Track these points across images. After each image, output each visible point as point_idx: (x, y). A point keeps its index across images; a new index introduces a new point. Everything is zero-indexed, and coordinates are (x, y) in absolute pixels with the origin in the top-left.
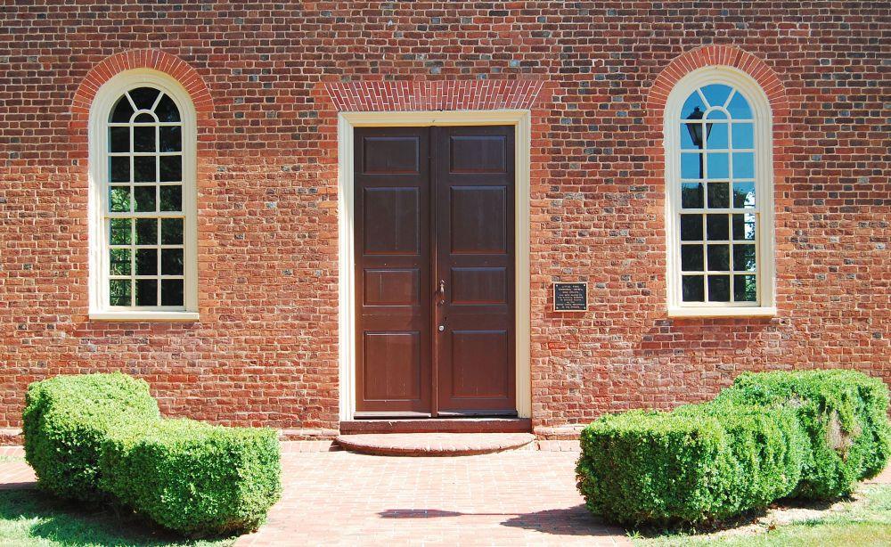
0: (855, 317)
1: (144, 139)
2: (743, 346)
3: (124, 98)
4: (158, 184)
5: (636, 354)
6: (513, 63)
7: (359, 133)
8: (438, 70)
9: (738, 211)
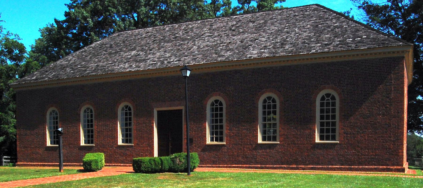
0: (240, 144)
1: (269, 107)
2: (219, 150)
3: (323, 96)
4: (325, 114)
5: (201, 152)
6: (182, 98)
7: (158, 112)
8: (169, 100)
9: (127, 127)
